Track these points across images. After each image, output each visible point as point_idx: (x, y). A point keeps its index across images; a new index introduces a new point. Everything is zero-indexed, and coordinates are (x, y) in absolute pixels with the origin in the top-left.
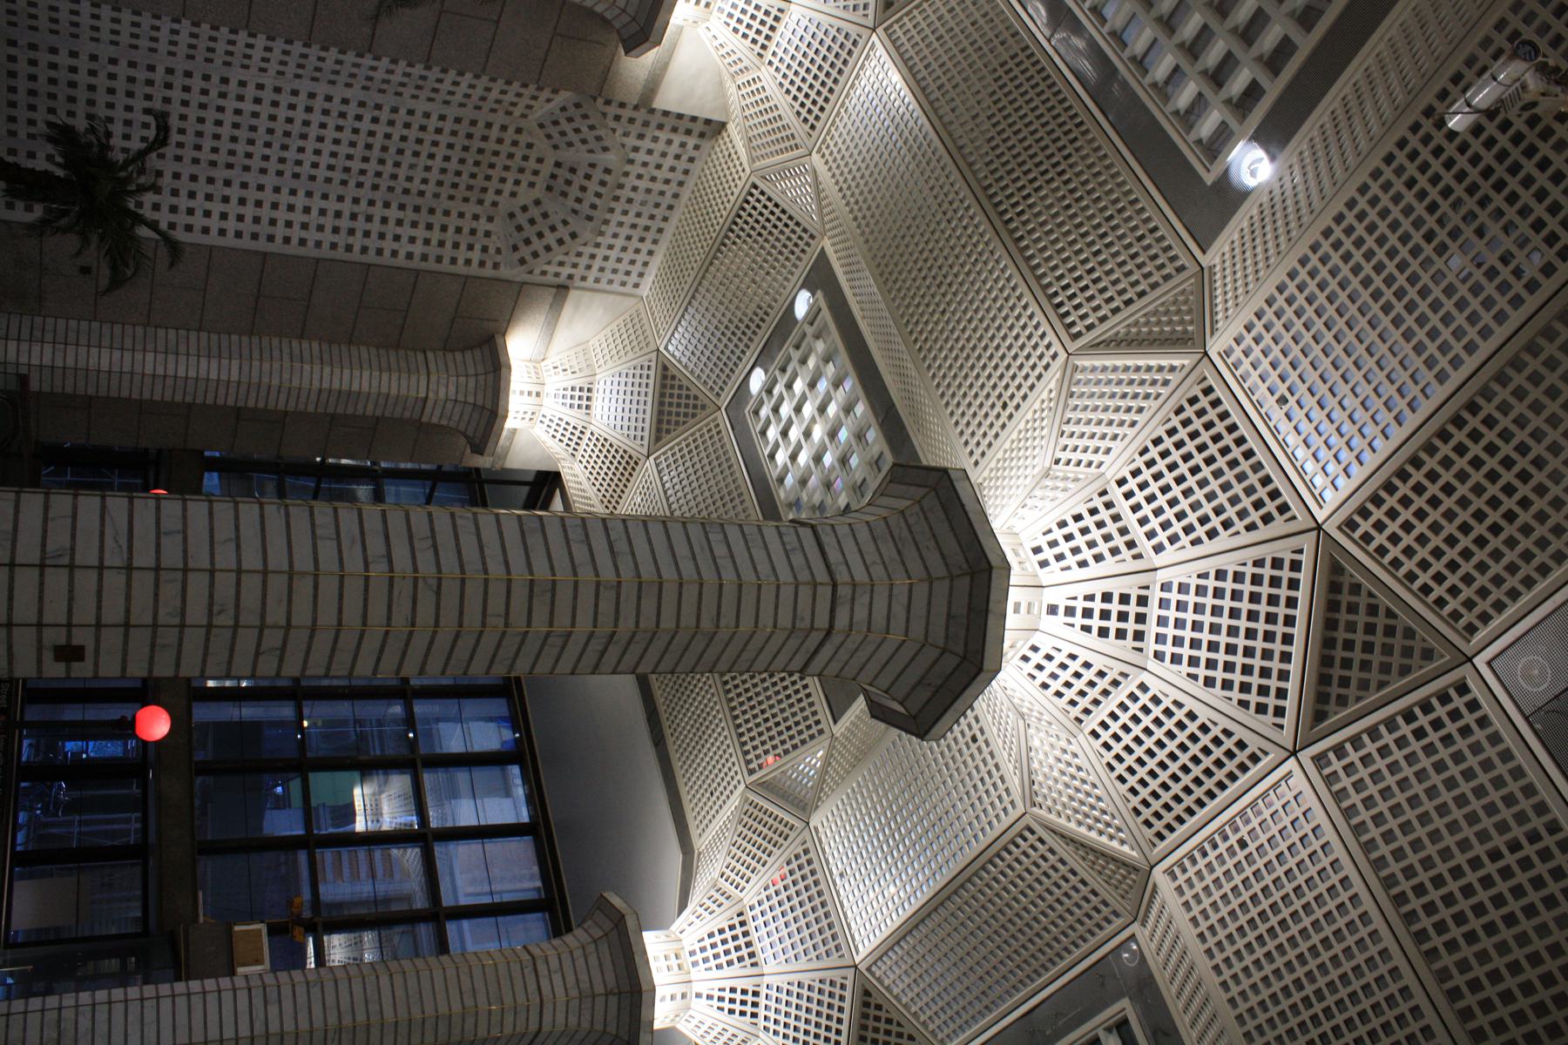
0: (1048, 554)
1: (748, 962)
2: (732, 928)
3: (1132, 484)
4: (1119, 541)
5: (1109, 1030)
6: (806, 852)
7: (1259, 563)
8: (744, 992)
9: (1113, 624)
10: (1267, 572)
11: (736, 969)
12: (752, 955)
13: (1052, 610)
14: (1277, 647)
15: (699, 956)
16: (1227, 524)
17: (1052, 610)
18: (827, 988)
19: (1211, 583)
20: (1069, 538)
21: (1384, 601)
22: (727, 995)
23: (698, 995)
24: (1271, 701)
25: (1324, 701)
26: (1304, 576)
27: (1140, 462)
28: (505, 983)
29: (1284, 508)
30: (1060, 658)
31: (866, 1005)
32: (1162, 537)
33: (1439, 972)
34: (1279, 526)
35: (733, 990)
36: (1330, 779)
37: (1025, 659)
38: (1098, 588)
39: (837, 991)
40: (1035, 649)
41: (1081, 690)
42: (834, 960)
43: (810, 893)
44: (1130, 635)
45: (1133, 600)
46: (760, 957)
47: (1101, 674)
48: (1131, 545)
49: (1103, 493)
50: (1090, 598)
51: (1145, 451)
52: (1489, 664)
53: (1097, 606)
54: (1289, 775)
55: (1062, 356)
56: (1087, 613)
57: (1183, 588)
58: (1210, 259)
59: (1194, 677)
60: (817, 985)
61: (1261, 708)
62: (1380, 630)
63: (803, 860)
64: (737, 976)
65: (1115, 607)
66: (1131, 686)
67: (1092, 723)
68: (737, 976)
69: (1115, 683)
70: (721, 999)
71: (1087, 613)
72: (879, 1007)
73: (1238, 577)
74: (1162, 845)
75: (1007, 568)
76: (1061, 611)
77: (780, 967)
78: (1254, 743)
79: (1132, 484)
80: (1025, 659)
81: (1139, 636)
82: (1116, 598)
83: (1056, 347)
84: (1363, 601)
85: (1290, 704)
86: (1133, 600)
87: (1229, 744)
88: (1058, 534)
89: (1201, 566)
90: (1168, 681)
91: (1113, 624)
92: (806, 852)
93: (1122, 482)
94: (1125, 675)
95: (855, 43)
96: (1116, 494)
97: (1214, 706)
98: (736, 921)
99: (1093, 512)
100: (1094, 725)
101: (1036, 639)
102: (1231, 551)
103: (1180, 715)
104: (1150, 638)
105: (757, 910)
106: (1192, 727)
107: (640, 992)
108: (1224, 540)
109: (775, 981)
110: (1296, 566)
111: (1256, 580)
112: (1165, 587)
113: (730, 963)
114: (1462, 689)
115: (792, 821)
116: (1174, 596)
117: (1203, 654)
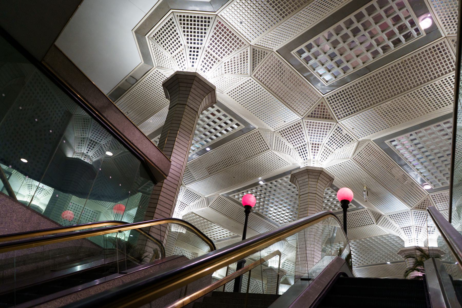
0: (305, 158)
3: (294, 144)
4: (196, 50)
7: (307, 127)
8: (312, 147)
9: (316, 148)
11: (412, 230)
20: (302, 155)
22: (313, 151)
23: (314, 158)
24: (329, 125)
25: (327, 117)
28: (303, 201)
29: (171, 19)
30: (322, 156)
31: (312, 116)
32: (303, 141)
34: (302, 124)
35: (312, 149)
36: (342, 118)
38: (311, 151)
39: (309, 123)
40: (202, 69)
41: (327, 152)
43: (397, 216)
63: (282, 133)
64: (309, 148)
65: (314, 148)
66: (327, 145)
67: (333, 151)
70: (315, 152)
72: (312, 113)
73: (309, 130)
76: (193, 64)
78: (216, 23)
79: (294, 144)
81: (318, 144)
83: (155, 70)
85: (329, 123)
89: (307, 135)
90: (326, 140)
92: (280, 132)
93: (294, 146)
94: (206, 51)
95: (338, 127)
96: (295, 147)
97: (330, 133)
99: (298, 150)
101: (319, 160)
102: (305, 131)
104: (319, 143)
108: (304, 132)
111: (310, 128)
114: (328, 98)
115: (383, 217)
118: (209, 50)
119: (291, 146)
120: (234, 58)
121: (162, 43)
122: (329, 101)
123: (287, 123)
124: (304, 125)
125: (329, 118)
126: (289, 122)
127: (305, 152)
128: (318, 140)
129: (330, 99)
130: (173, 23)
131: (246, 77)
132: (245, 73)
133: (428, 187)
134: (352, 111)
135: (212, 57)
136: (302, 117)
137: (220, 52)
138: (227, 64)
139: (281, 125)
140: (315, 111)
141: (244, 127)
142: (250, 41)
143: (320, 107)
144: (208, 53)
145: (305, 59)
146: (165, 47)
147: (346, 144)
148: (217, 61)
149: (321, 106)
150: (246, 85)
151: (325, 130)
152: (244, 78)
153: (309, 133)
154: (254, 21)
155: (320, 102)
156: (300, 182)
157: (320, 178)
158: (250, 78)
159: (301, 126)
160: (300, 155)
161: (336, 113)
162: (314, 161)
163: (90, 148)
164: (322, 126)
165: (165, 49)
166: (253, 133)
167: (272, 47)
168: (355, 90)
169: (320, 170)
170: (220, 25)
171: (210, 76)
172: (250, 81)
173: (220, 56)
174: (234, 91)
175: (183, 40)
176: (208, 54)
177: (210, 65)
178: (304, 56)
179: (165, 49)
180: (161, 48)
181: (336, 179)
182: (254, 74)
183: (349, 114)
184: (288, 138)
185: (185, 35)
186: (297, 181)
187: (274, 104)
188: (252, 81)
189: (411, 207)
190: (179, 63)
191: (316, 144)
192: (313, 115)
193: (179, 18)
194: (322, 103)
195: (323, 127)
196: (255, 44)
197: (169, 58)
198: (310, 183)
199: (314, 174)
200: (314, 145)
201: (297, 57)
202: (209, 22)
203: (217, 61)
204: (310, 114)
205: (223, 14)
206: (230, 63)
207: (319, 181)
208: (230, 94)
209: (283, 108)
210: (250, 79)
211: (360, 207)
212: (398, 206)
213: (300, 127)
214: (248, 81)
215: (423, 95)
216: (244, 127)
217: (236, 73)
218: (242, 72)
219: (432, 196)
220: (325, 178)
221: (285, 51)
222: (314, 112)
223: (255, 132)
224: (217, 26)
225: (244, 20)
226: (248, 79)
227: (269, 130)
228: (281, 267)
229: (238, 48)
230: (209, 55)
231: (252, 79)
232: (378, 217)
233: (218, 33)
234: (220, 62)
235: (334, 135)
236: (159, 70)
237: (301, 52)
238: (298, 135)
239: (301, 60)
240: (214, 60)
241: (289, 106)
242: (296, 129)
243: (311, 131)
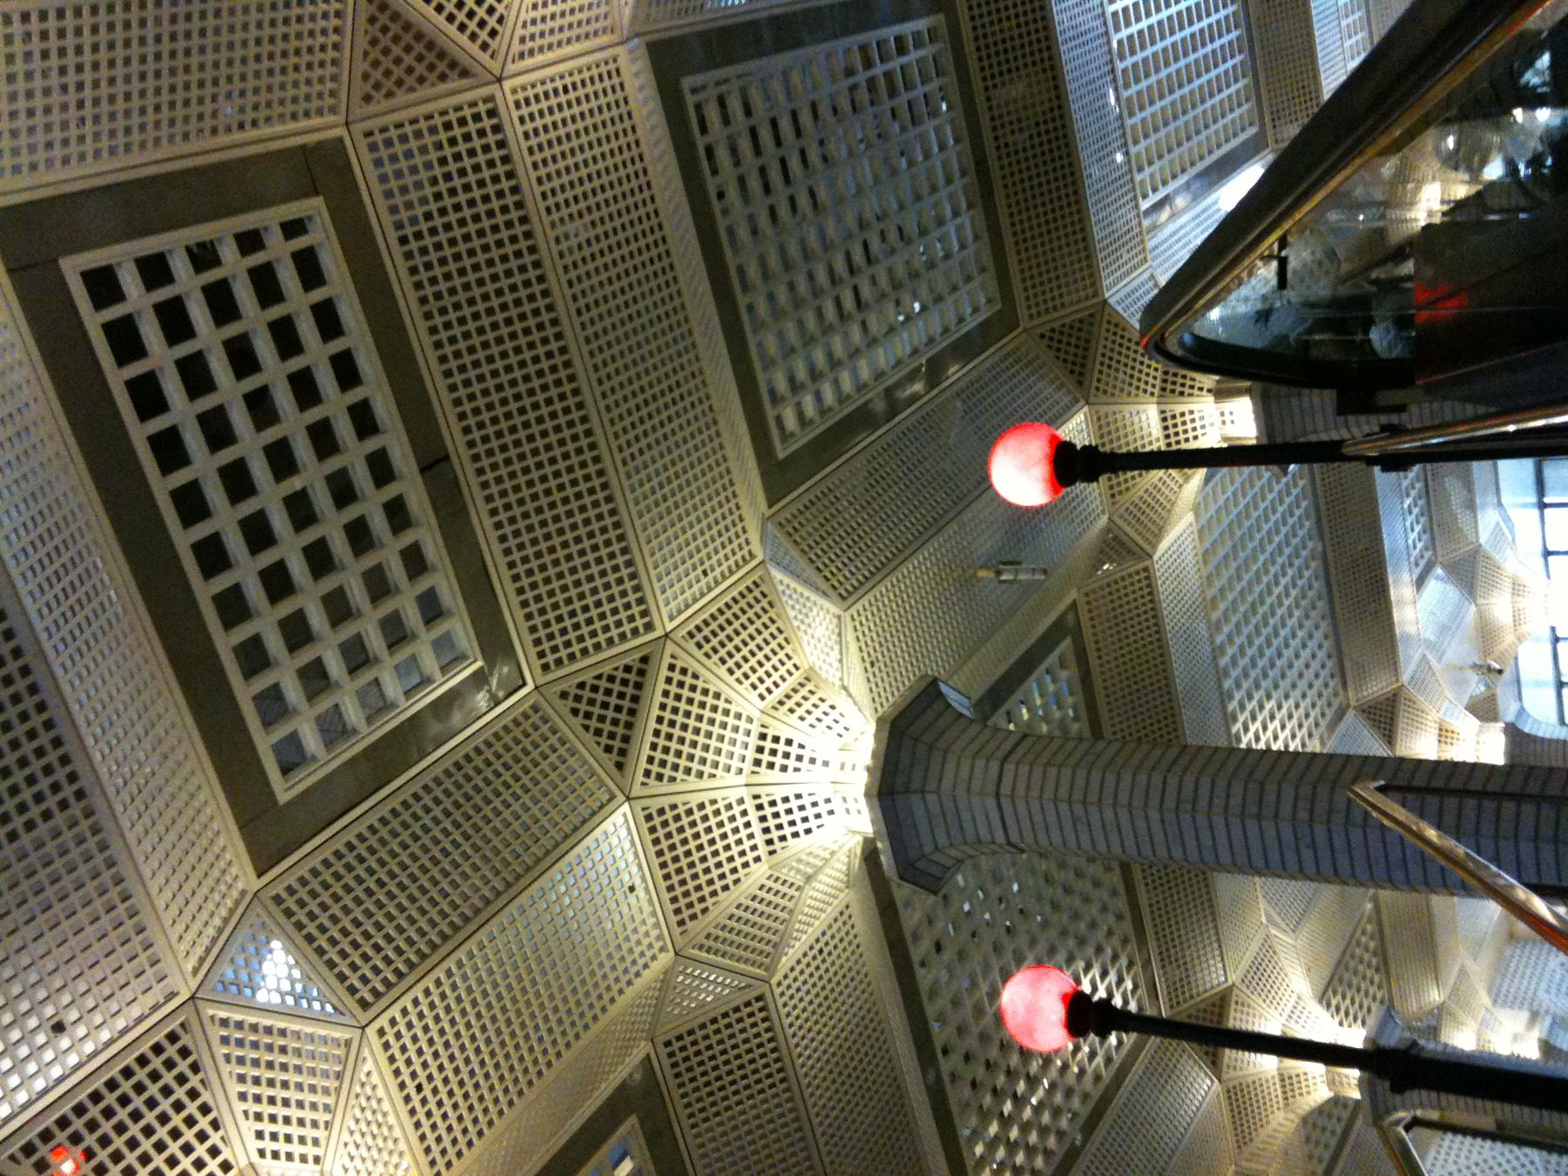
2: (746, 865)
3: (750, 856)
5: (314, 758)
7: (672, 779)
8: (771, 766)
9: (781, 747)
10: (667, 772)
15: (823, 808)
16: (689, 812)
18: (667, 772)
20: (805, 820)
23: (826, 764)
24: (676, 676)
27: (710, 901)
31: (623, 752)
34: (654, 805)
38: (790, 776)
39: (655, 769)
42: (1104, 409)
47: (792, 711)
48: (760, 807)
49: (772, 853)
51: (737, 882)
53: (792, 763)
54: (672, 618)
55: (774, 981)
60: (680, 775)
61: (684, 671)
63: (686, 914)
64: (776, 784)
65: (779, 760)
68: (776, 784)
69: (781, 703)
72: (608, 749)
73: (688, 771)
74: (755, 577)
75: (867, 795)
79: (750, 856)
81: (763, 737)
83: (778, 991)
85: (664, 673)
87: (707, 648)
88: (813, 823)
90: (745, 701)
91: (781, 747)
92: (681, 923)
93: (757, 859)
97: (715, 677)
100: (797, 674)
102: (690, 791)
103: (738, 673)
104: (755, 735)
106: (730, 663)
107: (880, 795)
108: (694, 800)
110: (647, 773)
111: (675, 767)
114: (546, 667)
119: (759, 872)
122: (559, 662)
123: (638, 882)
124: (661, 794)
125: (641, 673)
126: (634, 869)
127: (794, 804)
128: (740, 737)
129: (550, 658)
131: (366, 1053)
134: (628, 585)
136: (621, 797)
138: (269, 1146)
139: (647, 909)
140: (598, 732)
141: (633, 1120)
142: (173, 995)
143: (583, 707)
145: (329, 744)
147: (772, 614)
149: (581, 699)
150: (404, 1049)
151: (698, 697)
153: (700, 775)
154: (65, 952)
155: (558, 702)
156: (942, 840)
158: (371, 1031)
159: (661, 812)
160: (808, 831)
161: (623, 636)
162: (842, 767)
163: (799, 758)
164: (675, 711)
166: (669, 1073)
167: (235, 894)
168: (521, 524)
174: (431, 1137)
178: (311, 741)
182: (357, 1010)
183: (641, 601)
184: (718, 885)
186: (936, 857)
187: (535, 928)
188: (393, 1022)
189: (612, 797)
191: (760, 750)
192: (617, 744)
194: (367, 98)
195: (683, 706)
198: (947, 784)
199: (905, 758)
200: (766, 758)
201: (306, 779)
204: (609, 760)
206: (267, 1128)
209: (561, 885)
210: (381, 1032)
213: (669, 815)
214: (387, 1046)
215: (770, 910)
216: (633, 1120)
221: (268, 832)
222: (604, 740)
223: (666, 1062)
225: (49, 1011)
226: (376, 1043)
227: (668, 973)
228: (1355, 1037)
229: (195, 1068)
231: (383, 1021)
235: (723, 661)
237: (292, 757)
238: (709, 830)
239: (324, 762)
242: (687, 874)
243: (695, 766)
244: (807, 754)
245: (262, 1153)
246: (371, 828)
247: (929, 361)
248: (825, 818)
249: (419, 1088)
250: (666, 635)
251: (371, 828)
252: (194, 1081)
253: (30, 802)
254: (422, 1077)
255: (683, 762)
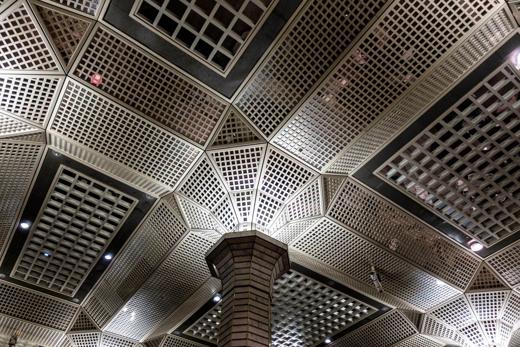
1: (475, 326)
4: (224, 205)
6: (434, 313)
7: (219, 165)
9: (246, 201)
11: (479, 330)
12: (473, 326)
13: (245, 219)
14: (240, 154)
17: (245, 219)
18: (474, 300)
19: (228, 176)
21: (221, 130)
23: (493, 341)
26: (219, 152)
29: (204, 162)
33: (240, 33)
34: (465, 299)
37: (263, 224)
38: (485, 332)
39: (474, 297)
40: (259, 222)
43: (448, 310)
44: (248, 196)
45: (238, 197)
46: (473, 323)
50: (240, 209)
52: (230, 99)
53: (242, 207)
56: (244, 209)
57: (231, 184)
58: (157, 196)
59: (255, 175)
62: (229, 129)
63: (437, 313)
64: (482, 329)
66: (264, 192)
68: (482, 329)
71: (244, 209)
73: (477, 305)
76: (245, 217)
77: (473, 315)
78: (269, 154)
80: (263, 224)
82: (239, 202)
83: (190, 234)
84: (222, 135)
86: (238, 197)
92: (434, 313)
93: (457, 327)
94: (261, 194)
97: (504, 305)
98: (463, 332)
105: (458, 325)
109: (478, 317)
110: (217, 155)
111: (476, 302)
112: (232, 189)
113: (478, 332)
116: (234, 186)
117: (248, 174)
118: (264, 192)
120: (301, 196)
121: (194, 197)
130: (207, 165)
132: (317, 214)
133: (478, 247)
135: (270, 202)
137: (280, 192)
138: (292, 207)
140: (478, 280)
144: (264, 196)
146: (189, 193)
148: (278, 206)
150: (319, 230)
152: (316, 221)
157: (255, 253)
158: (324, 218)
165: (189, 196)
169: (250, 234)
170: (275, 156)
171: (274, 229)
172: (324, 223)
173: (282, 198)
175: (225, 186)
176: (264, 199)
177: (270, 213)
179: (189, 196)
180: (194, 204)
181: (291, 248)
184: (469, 334)
185: (226, 178)
189: (463, 288)
190: (224, 219)
193: (215, 157)
196: (327, 172)
197: (207, 214)
201: (381, 177)
202: (258, 154)
203: (278, 206)
205: (277, 140)
207: (254, 259)
208: (298, 245)
210: (325, 221)
211: (384, 309)
212: (440, 291)
217: (306, 216)
218: (313, 213)
219: (490, 262)
220: (268, 252)
221: (366, 174)
222: (477, 282)
224: (271, 157)
230: (266, 200)
231: (328, 220)
232: (417, 318)
233: (273, 168)
234: (283, 206)
236: (195, 233)
239: (387, 178)
240: (274, 204)
241: (418, 266)
244: (493, 335)
245: (289, 206)
246: (352, 184)
247: (447, 223)
248: (208, 207)
249: (314, 234)
250: (268, 143)
251: (352, 184)
252: (301, 183)
253: (287, 67)
254: (317, 234)
255: (478, 303)
